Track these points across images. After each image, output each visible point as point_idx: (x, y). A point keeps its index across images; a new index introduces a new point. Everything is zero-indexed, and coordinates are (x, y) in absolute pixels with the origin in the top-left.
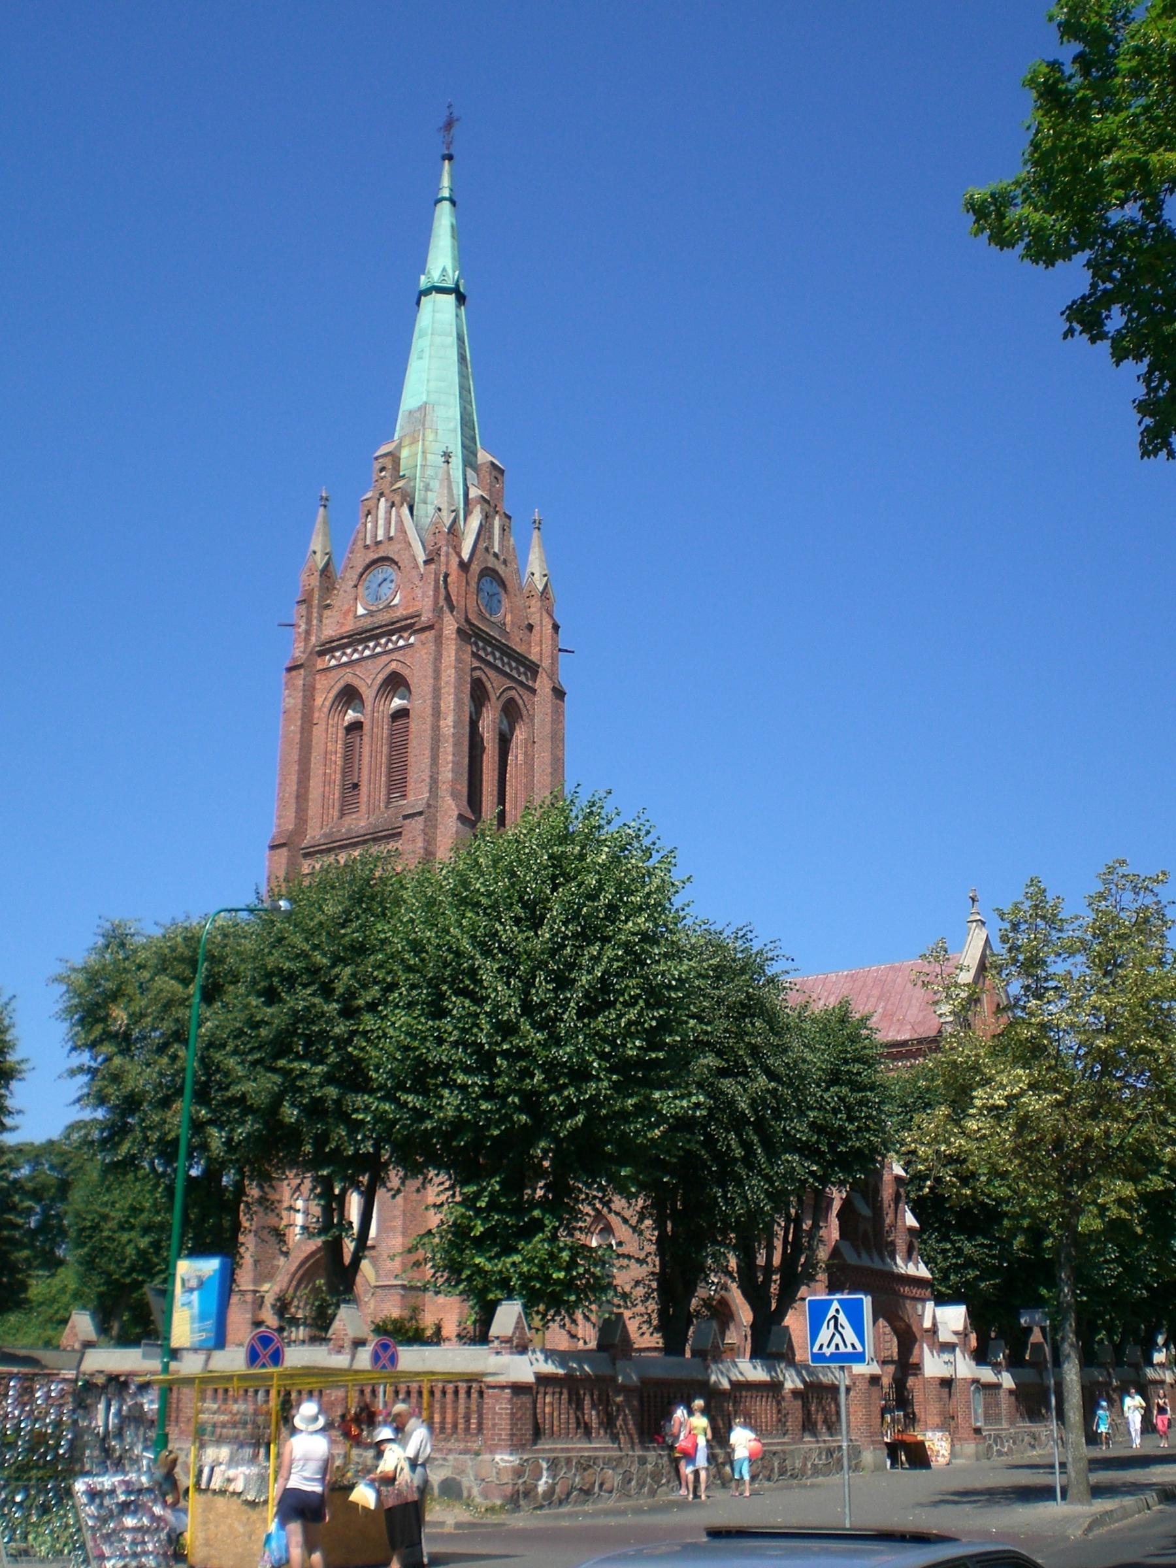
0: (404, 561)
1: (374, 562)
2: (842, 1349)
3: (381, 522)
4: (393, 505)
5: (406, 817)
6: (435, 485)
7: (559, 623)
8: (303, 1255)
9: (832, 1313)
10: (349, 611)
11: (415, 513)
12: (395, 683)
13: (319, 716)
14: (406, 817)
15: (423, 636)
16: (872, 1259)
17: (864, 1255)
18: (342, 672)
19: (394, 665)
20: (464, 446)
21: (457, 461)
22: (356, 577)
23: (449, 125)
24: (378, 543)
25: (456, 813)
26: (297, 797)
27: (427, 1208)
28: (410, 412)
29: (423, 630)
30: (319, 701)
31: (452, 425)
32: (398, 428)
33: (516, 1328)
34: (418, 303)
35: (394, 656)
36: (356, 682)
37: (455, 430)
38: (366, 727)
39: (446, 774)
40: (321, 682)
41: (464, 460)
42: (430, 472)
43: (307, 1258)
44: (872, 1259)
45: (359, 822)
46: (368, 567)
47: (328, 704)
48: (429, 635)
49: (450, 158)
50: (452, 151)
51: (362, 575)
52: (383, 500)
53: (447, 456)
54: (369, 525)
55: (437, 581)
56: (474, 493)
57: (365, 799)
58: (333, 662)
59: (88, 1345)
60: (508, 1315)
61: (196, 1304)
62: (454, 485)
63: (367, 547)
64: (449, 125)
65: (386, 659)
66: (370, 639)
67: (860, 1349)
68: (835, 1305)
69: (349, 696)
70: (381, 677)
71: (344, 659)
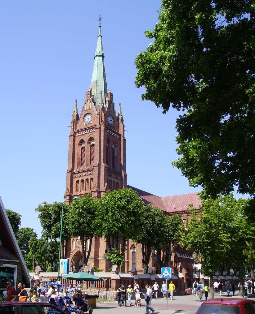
0: (93, 113)
1: (87, 114)
2: (167, 276)
3: (88, 106)
4: (90, 102)
5: (94, 167)
6: (99, 97)
7: (125, 125)
8: (75, 253)
9: (165, 270)
10: (81, 124)
11: (96, 106)
12: (91, 139)
13: (76, 145)
14: (94, 167)
15: (97, 130)
16: (185, 256)
17: (181, 255)
18: (81, 136)
19: (91, 136)
20: (105, 89)
21: (103, 93)
22: (83, 117)
23: (100, 19)
24: (87, 110)
25: (104, 166)
26: (72, 162)
27: (98, 36)
28: (93, 82)
29: (97, 128)
30: (76, 143)
31: (102, 85)
32: (91, 85)
33: (116, 269)
34: (95, 58)
35: (91, 133)
36: (83, 139)
37: (103, 86)
38: (86, 148)
39: (102, 158)
40: (77, 139)
41: (105, 92)
42: (98, 95)
43: (76, 253)
44: (185, 256)
45: (85, 167)
46: (85, 115)
47: (78, 143)
48: (99, 129)
49: (100, 26)
50: (101, 25)
51: (84, 116)
52: (88, 101)
53: (101, 92)
54: (86, 106)
55: (100, 119)
56: (107, 99)
57: (86, 163)
58: (79, 134)
59: (40, 272)
60: (115, 267)
61: (64, 267)
62: (103, 97)
63: (85, 111)
64: (100, 19)
65: (89, 134)
66: (86, 130)
67: (170, 276)
68: (166, 269)
69: (82, 142)
70: (89, 138)
71: (81, 134)
